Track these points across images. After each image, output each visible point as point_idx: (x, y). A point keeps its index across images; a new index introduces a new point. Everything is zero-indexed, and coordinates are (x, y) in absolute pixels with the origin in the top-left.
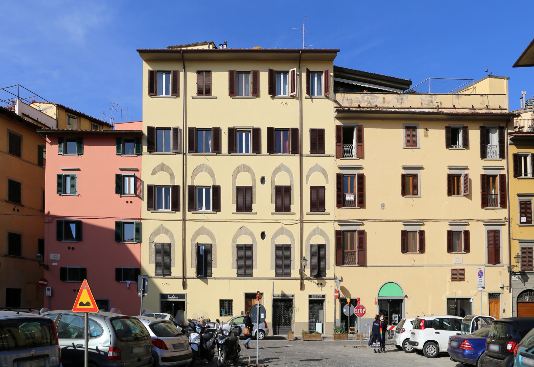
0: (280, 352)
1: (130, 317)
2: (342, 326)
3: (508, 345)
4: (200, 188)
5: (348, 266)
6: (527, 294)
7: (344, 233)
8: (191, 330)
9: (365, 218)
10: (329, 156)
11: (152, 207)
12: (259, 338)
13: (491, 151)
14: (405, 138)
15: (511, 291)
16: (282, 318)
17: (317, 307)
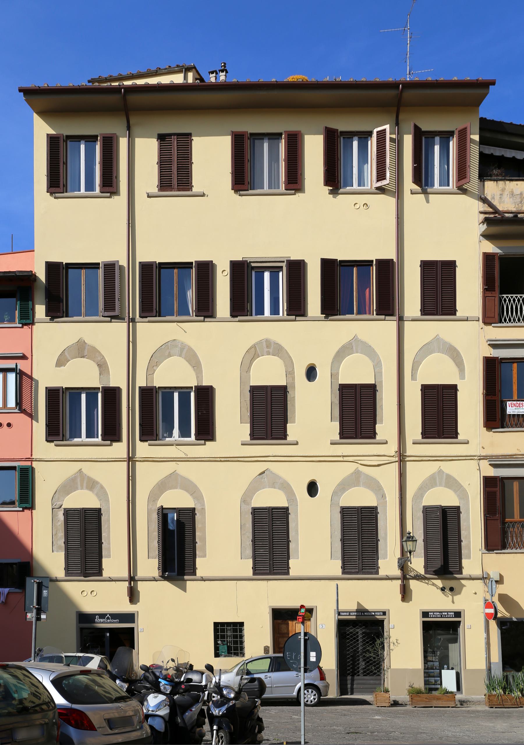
0: (357, 733)
1: (8, 665)
4: (168, 392)
5: (514, 550)
8: (147, 689)
10: (467, 320)
11: (58, 435)
12: (307, 701)
16: (359, 660)
17: (442, 637)
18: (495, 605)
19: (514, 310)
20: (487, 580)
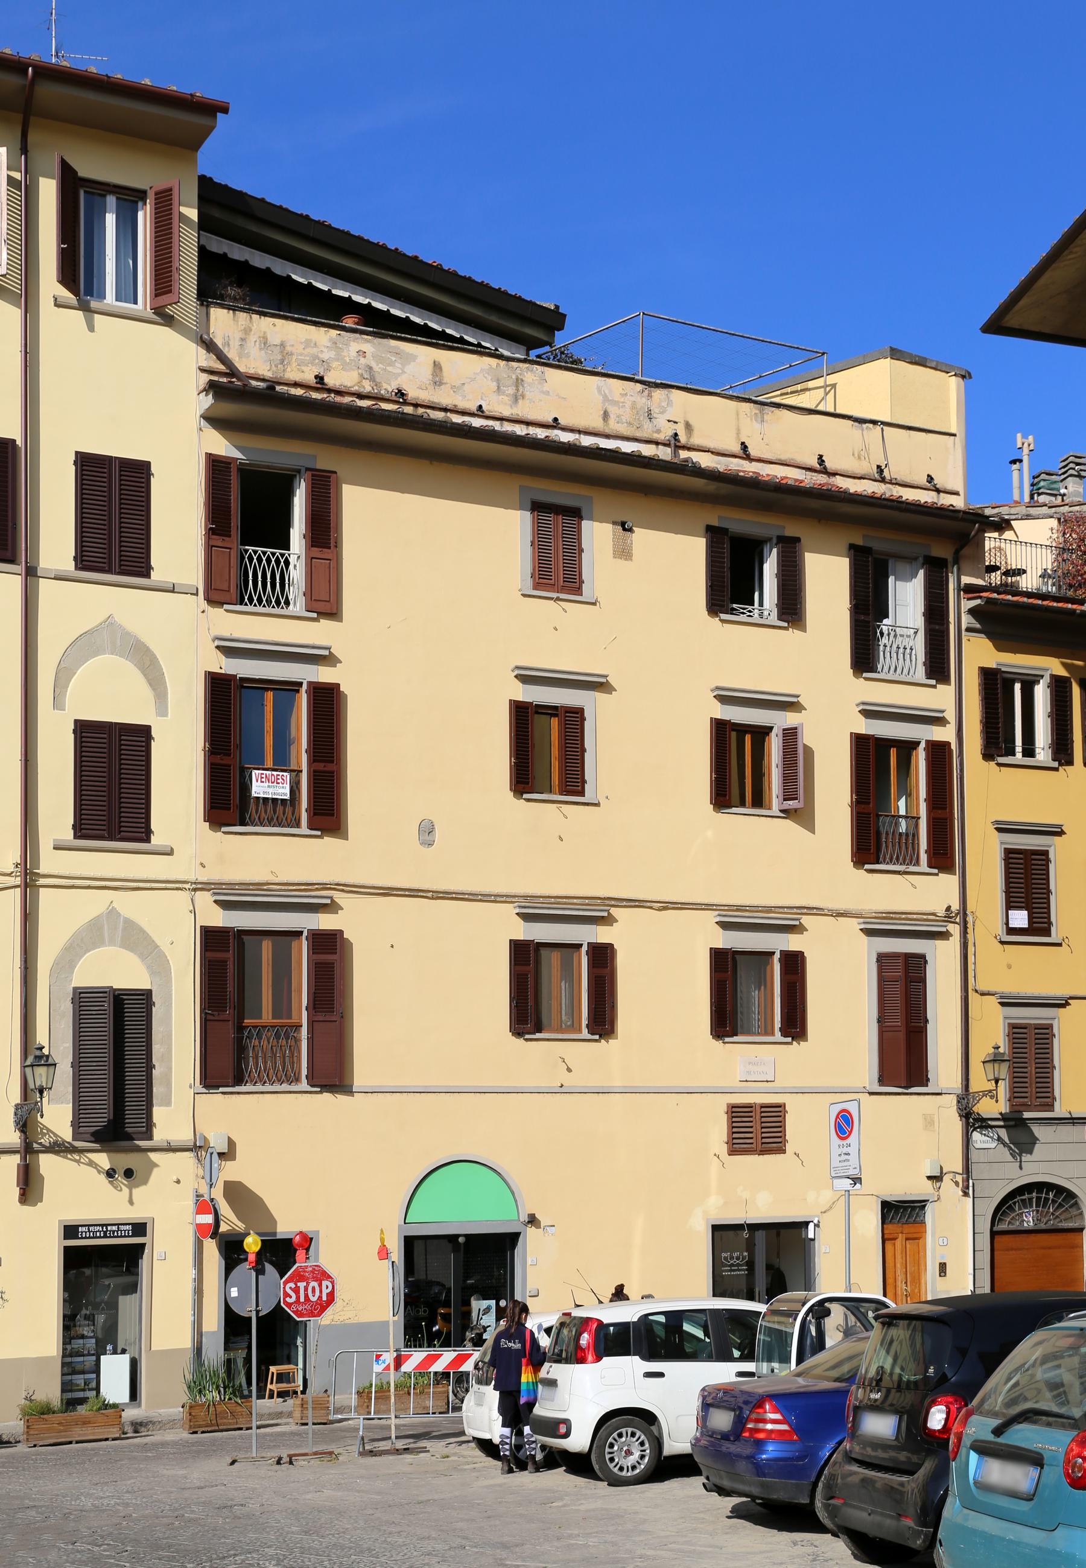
2: (229, 1363)
3: (933, 1410)
5: (259, 1087)
6: (1031, 1199)
7: (244, 943)
9: (343, 881)
10: (173, 591)
13: (895, 647)
14: (529, 550)
15: (971, 1189)
18: (216, 1206)
19: (269, 580)
20: (203, 1152)
